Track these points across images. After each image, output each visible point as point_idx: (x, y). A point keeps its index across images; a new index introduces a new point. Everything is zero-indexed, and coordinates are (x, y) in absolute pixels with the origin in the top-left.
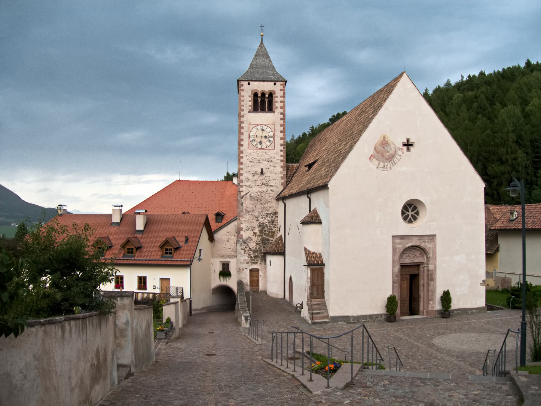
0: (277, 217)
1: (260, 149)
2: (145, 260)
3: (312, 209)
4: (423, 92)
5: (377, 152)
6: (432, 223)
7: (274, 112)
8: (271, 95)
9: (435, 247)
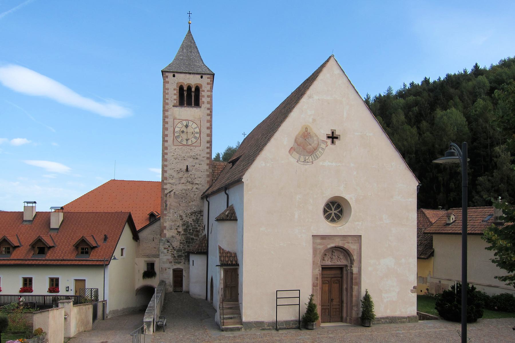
0: (203, 216)
2: (97, 261)
3: (230, 205)
4: (364, 97)
6: (357, 223)
7: (201, 107)
8: (198, 89)
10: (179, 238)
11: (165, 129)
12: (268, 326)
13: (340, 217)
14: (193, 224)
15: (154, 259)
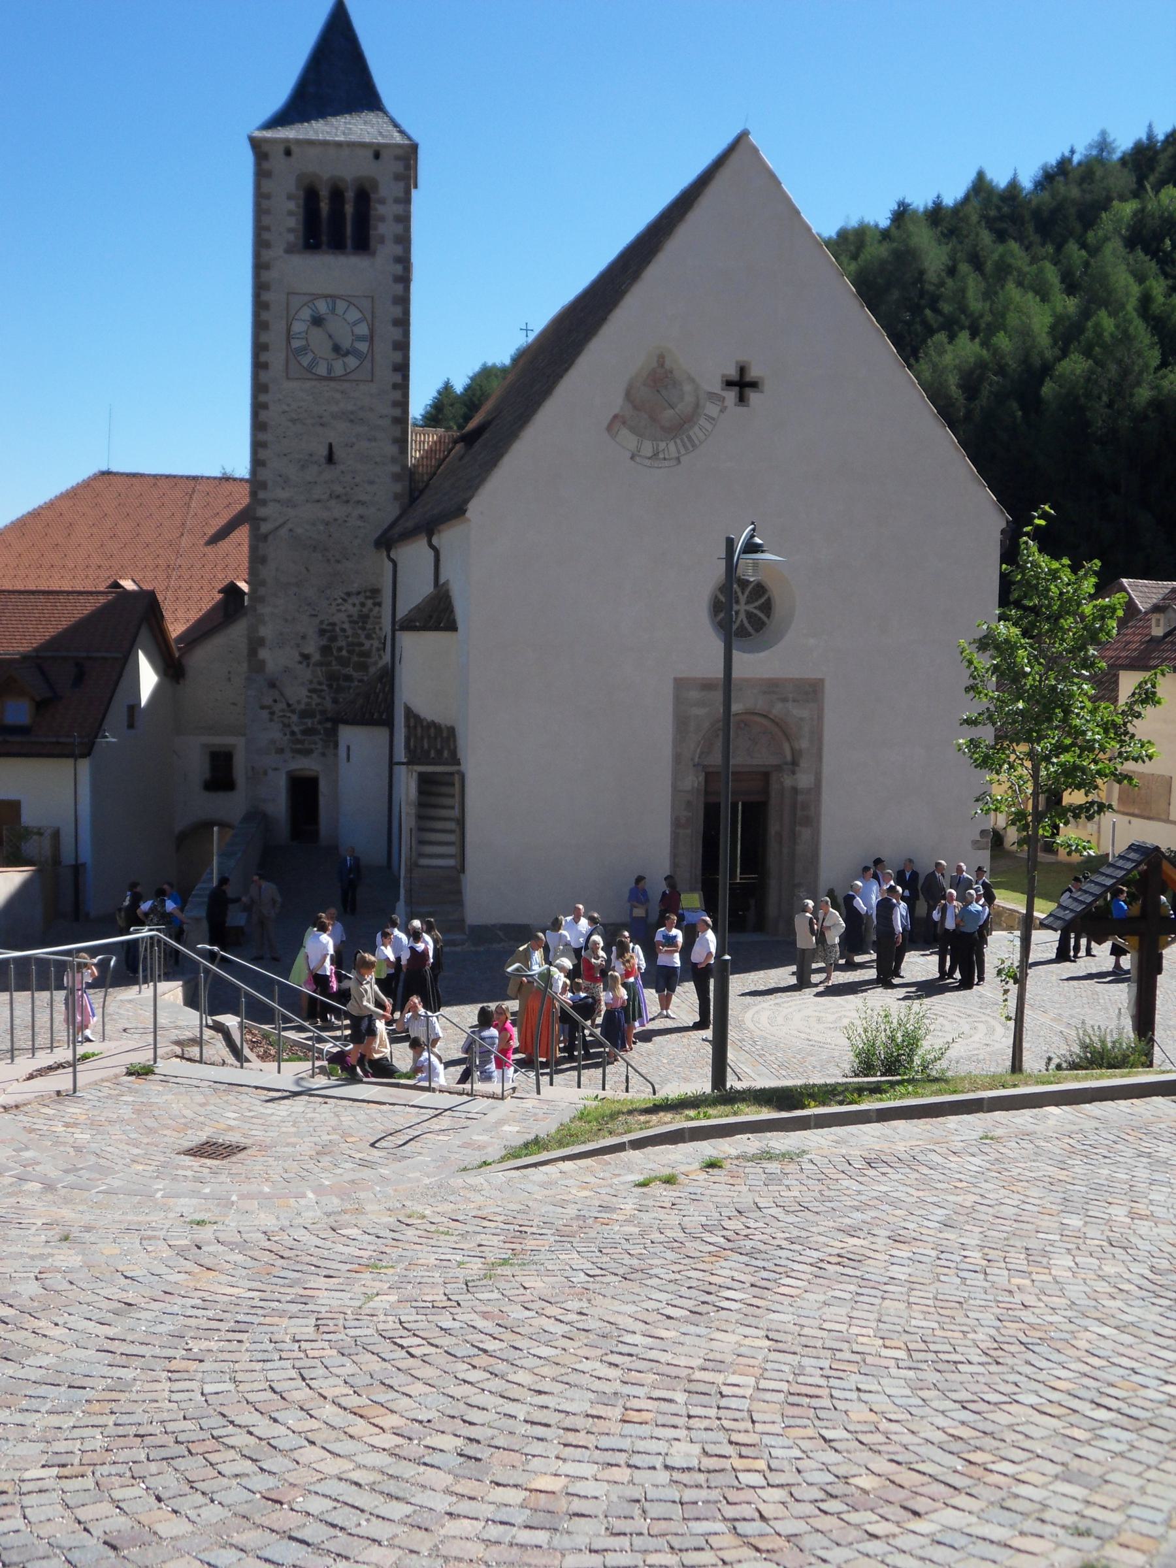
1: (322, 378)
5: (635, 408)
7: (373, 254)
8: (364, 196)
9: (820, 718)
13: (763, 624)
14: (349, 632)
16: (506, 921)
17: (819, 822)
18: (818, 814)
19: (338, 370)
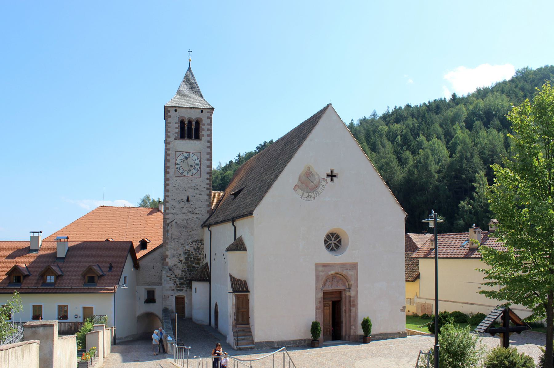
0: (203, 244)
5: (302, 183)
6: (354, 251)
7: (201, 140)
8: (198, 123)
9: (357, 274)
10: (180, 266)
11: (166, 161)
12: (278, 345)
14: (194, 253)
15: (154, 287)
16: (266, 340)
17: (357, 305)
18: (357, 304)
19: (190, 174)
